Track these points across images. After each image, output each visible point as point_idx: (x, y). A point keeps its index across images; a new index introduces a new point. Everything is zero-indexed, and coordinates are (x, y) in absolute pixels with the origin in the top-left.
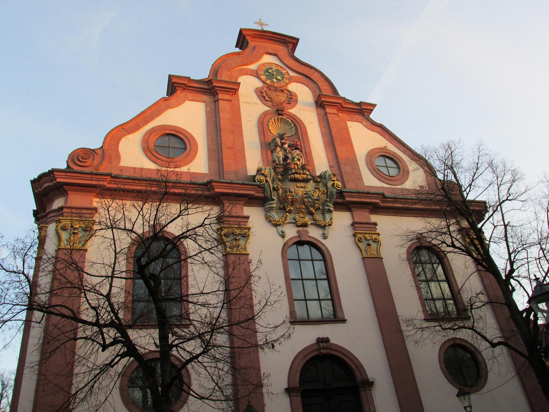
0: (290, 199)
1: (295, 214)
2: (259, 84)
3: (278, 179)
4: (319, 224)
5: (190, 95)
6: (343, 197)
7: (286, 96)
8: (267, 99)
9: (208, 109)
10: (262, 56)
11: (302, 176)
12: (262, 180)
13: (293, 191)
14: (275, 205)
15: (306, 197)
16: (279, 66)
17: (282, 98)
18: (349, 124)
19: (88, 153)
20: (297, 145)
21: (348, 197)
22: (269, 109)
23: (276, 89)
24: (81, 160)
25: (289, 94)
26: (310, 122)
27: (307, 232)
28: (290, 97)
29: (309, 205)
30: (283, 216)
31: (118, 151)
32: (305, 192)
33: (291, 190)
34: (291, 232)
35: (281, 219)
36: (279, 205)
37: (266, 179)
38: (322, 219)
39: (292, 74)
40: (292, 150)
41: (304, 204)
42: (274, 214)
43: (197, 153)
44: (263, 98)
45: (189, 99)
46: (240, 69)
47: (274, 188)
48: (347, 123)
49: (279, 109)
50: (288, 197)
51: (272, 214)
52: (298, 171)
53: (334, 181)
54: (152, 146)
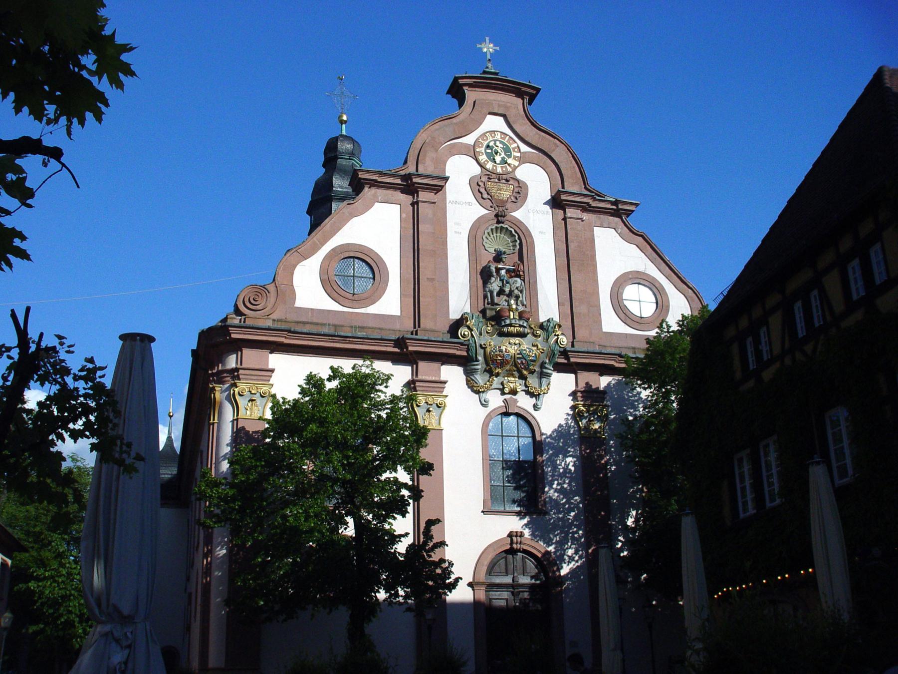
0: (499, 360)
1: (503, 377)
2: (477, 170)
3: (487, 332)
4: (532, 391)
5: (380, 193)
6: (567, 358)
7: (512, 189)
8: (485, 196)
9: (404, 216)
10: (486, 116)
11: (517, 330)
12: (465, 335)
13: (504, 350)
14: (479, 367)
15: (519, 358)
16: (507, 135)
17: (505, 192)
18: (597, 231)
19: (260, 291)
20: (519, 271)
21: (572, 357)
22: (487, 212)
23: (499, 177)
24: (252, 301)
25: (517, 185)
26: (541, 232)
27: (516, 401)
28: (516, 190)
29: (523, 367)
30: (489, 381)
31: (293, 285)
32: (519, 351)
33: (502, 348)
34: (495, 400)
35: (486, 384)
36: (485, 366)
37: (472, 334)
38: (537, 386)
39: (524, 148)
40: (511, 277)
41: (516, 366)
42: (477, 378)
43: (387, 285)
44: (480, 195)
45: (380, 201)
46: (449, 144)
47: (481, 346)
48: (593, 231)
49: (500, 213)
50: (497, 357)
51: (474, 377)
52: (513, 322)
53: (558, 335)
54: (332, 273)
